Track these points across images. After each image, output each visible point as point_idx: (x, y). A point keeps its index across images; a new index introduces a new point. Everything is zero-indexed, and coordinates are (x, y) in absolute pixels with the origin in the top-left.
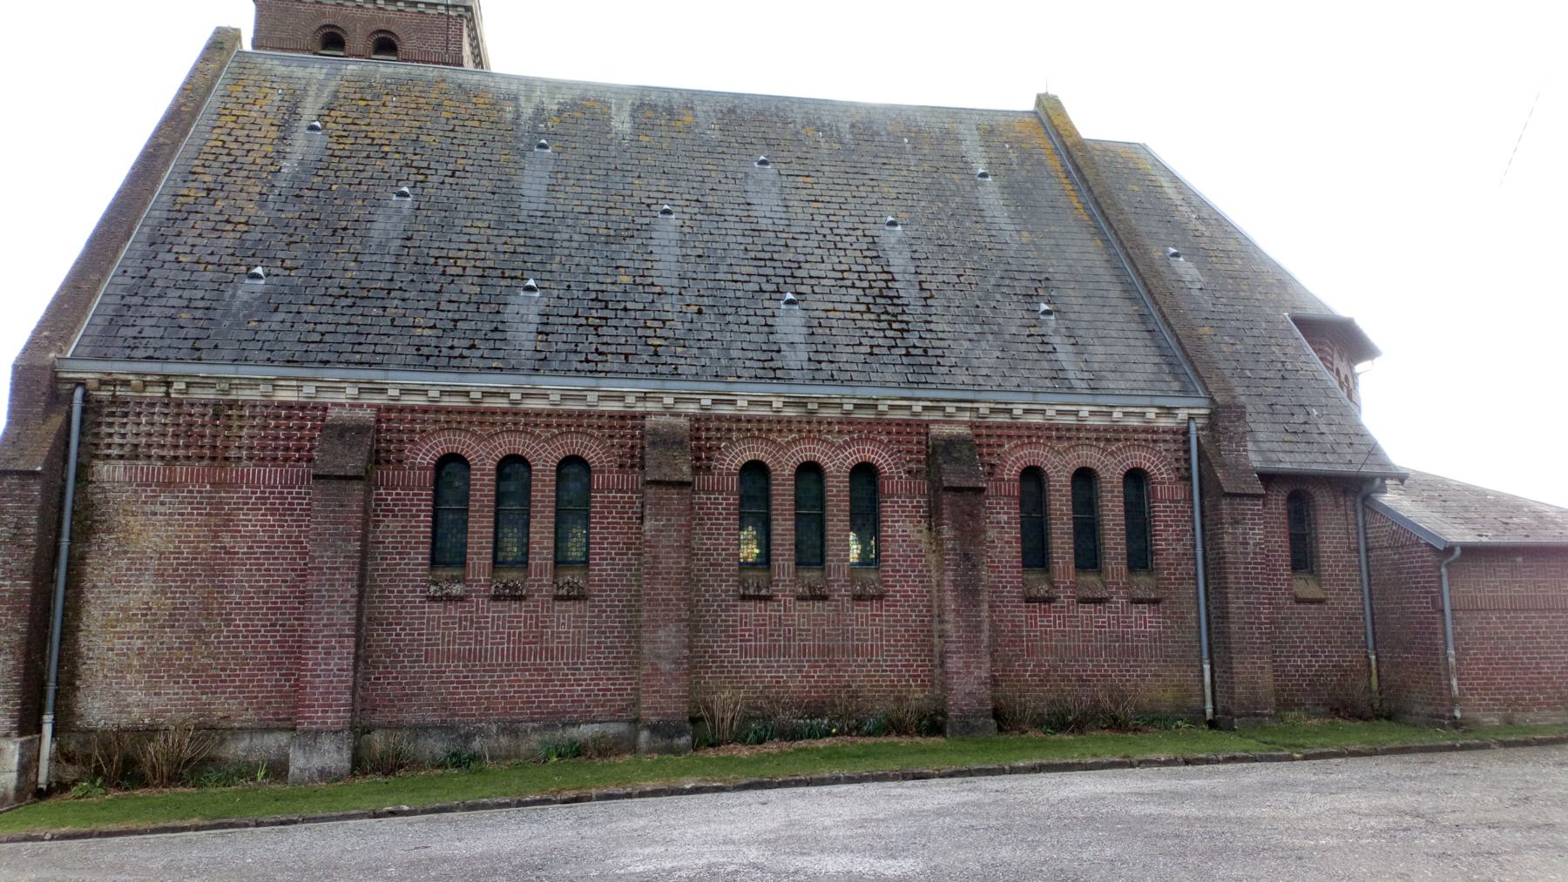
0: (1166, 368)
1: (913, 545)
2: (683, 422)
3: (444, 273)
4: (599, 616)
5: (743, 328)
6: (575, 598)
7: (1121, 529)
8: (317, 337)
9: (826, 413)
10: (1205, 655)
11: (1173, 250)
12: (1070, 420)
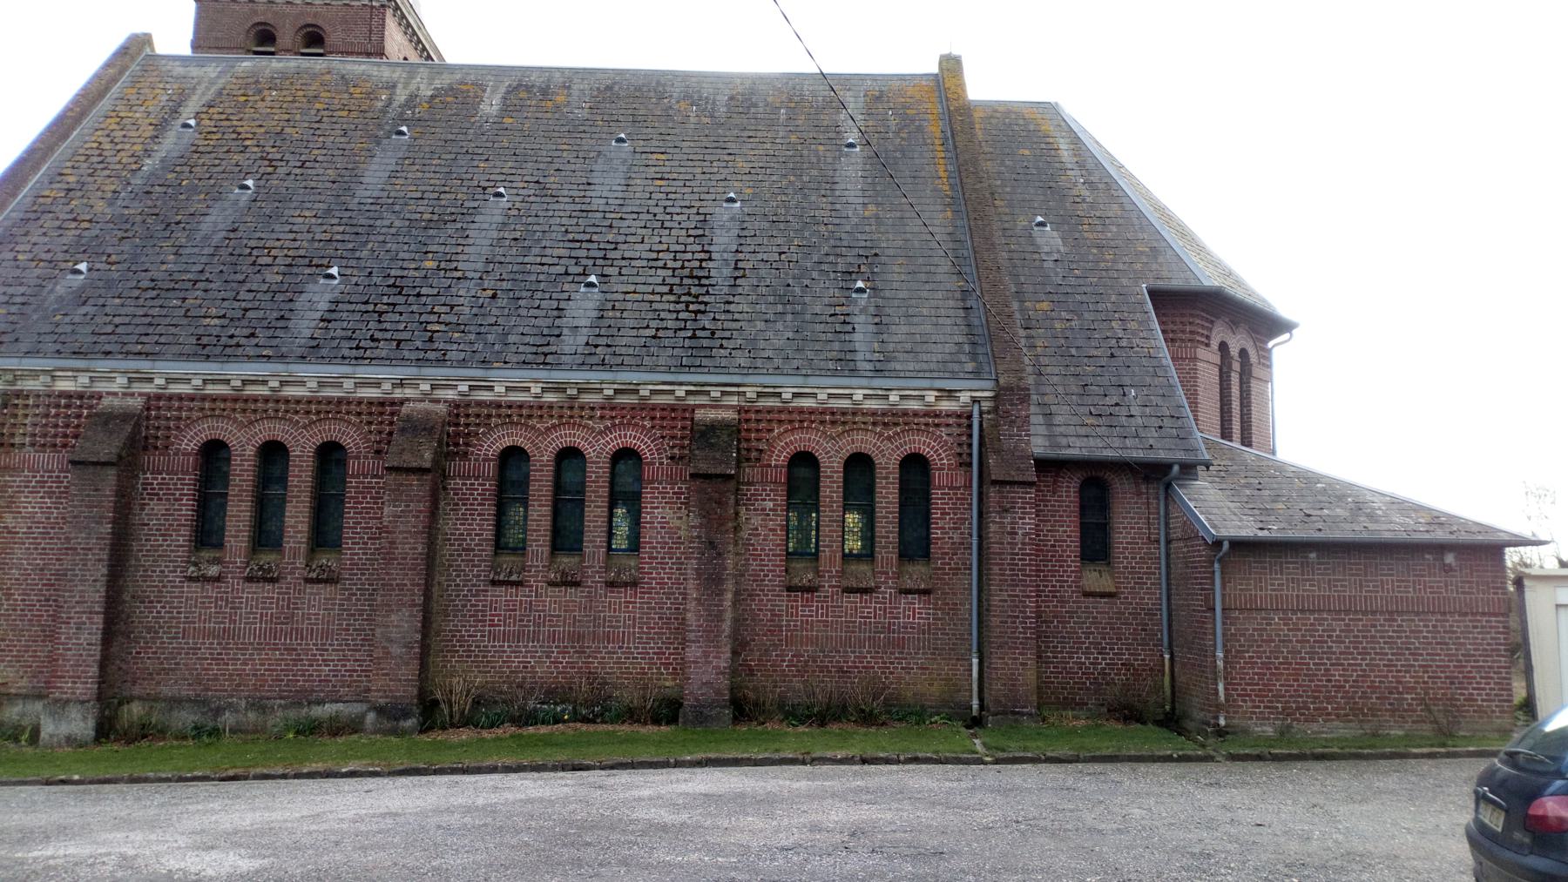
0: (967, 348)
1: (672, 532)
2: (441, 408)
3: (254, 264)
4: (349, 599)
5: (533, 312)
6: (326, 581)
7: (894, 517)
8: (109, 329)
9: (587, 398)
10: (975, 649)
11: (1040, 219)
12: (845, 404)
